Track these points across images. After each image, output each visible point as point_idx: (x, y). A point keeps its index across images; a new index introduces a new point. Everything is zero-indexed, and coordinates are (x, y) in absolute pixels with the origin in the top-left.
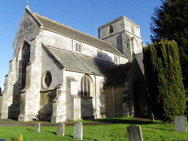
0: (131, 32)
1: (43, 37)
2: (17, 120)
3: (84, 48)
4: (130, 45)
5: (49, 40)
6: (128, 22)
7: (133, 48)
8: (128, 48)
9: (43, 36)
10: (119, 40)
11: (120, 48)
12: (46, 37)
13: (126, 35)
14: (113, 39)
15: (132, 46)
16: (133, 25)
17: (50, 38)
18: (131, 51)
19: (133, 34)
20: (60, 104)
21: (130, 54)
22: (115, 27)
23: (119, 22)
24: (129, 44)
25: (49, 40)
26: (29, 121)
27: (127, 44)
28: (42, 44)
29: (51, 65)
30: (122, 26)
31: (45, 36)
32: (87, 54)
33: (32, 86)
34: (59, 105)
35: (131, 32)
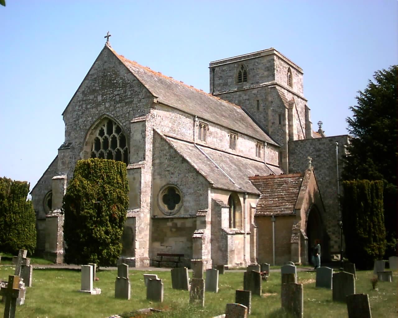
0: (285, 85)
1: (155, 118)
2: (135, 267)
3: (211, 133)
4: (284, 119)
5: (162, 123)
6: (282, 62)
7: (290, 126)
8: (280, 123)
9: (155, 116)
10: (260, 102)
11: (263, 121)
12: (159, 117)
13: (279, 96)
14: (247, 97)
15: (289, 121)
16: (291, 68)
17: (164, 119)
18: (287, 131)
19: (290, 89)
20: (206, 242)
21: (285, 138)
22: (251, 69)
23: (265, 60)
24: (284, 115)
25: (162, 123)
26: (4, 308)
27: (280, 116)
28: (154, 130)
29: (179, 174)
30: (268, 70)
31: (158, 116)
32: (214, 145)
33: (143, 208)
34: (204, 244)
35: (285, 85)
